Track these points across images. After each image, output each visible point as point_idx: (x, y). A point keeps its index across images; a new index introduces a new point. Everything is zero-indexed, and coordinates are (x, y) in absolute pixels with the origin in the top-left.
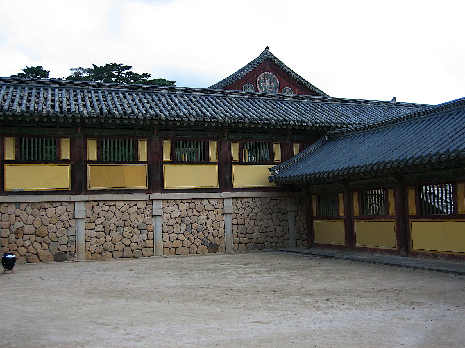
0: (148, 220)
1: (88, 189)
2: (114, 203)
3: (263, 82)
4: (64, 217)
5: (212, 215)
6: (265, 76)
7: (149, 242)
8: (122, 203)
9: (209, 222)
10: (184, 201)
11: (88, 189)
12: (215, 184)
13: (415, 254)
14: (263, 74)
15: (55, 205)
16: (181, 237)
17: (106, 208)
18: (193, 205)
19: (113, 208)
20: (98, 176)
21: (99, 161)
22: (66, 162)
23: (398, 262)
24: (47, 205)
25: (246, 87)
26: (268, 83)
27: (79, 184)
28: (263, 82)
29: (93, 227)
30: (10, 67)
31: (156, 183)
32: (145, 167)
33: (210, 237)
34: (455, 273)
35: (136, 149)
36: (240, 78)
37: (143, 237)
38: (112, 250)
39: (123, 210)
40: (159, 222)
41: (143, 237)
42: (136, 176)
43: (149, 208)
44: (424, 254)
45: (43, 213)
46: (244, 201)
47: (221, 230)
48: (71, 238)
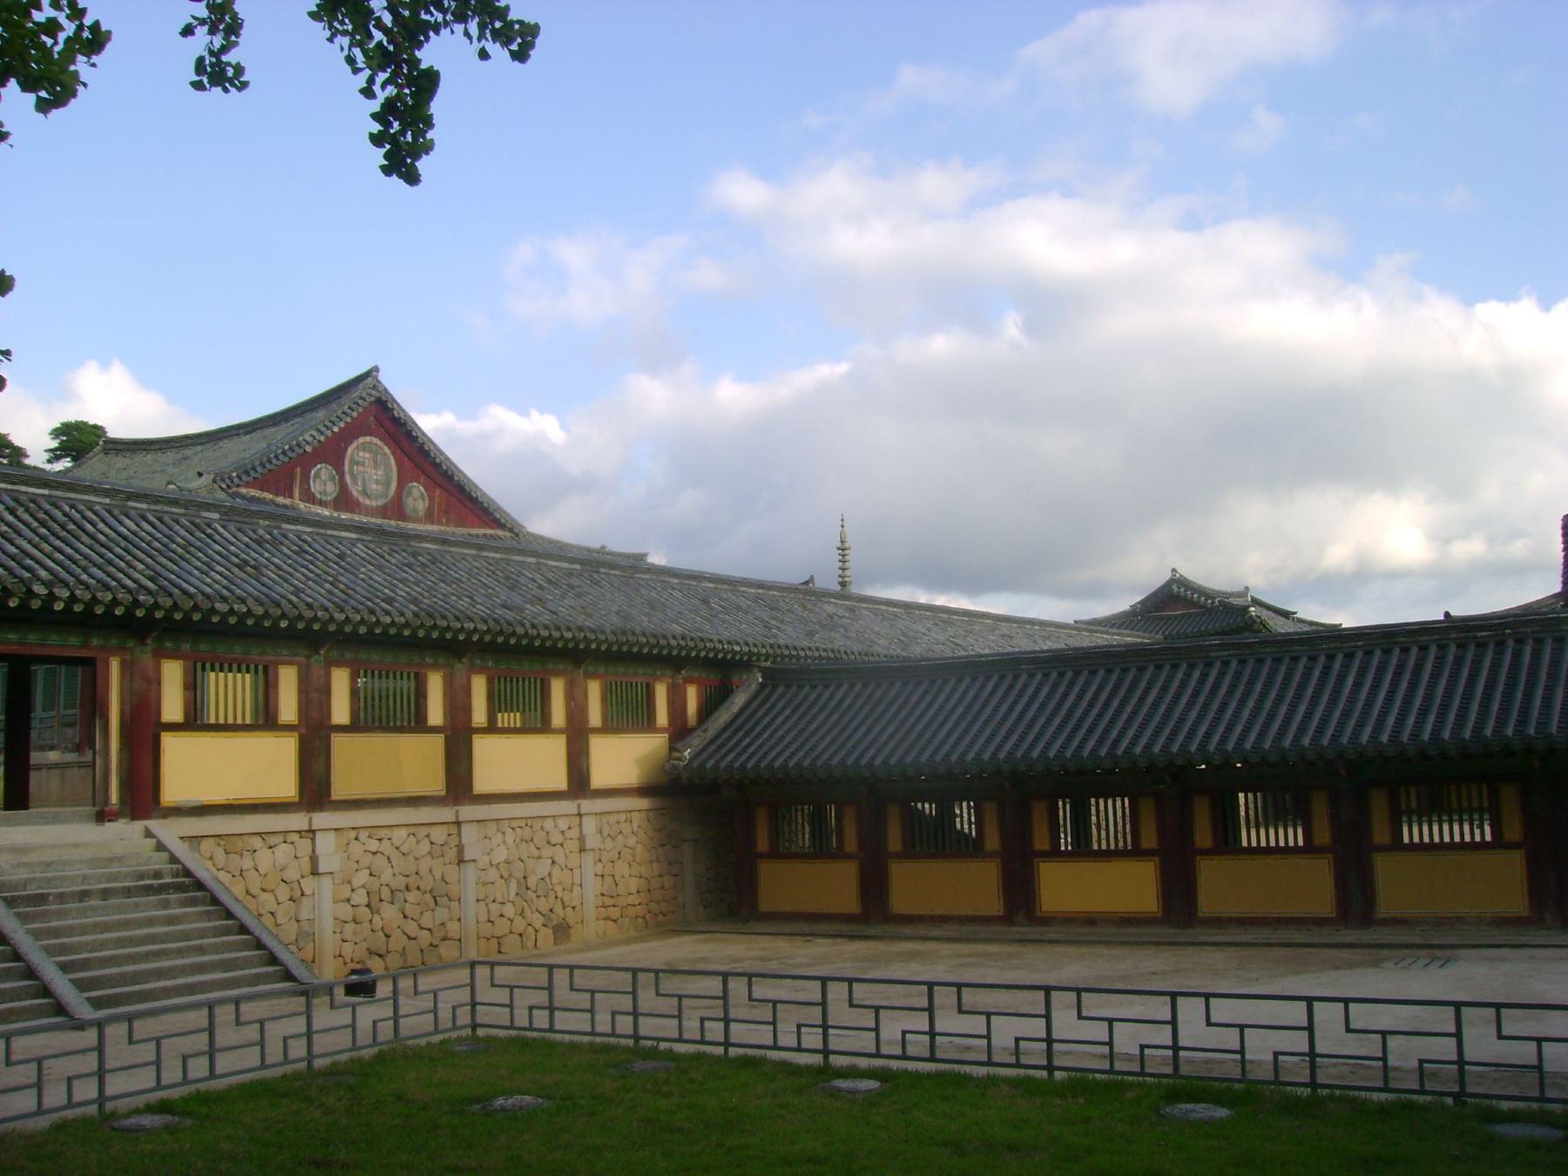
0: (452, 872)
1: (334, 797)
2: (388, 832)
3: (358, 463)
4: (292, 874)
5: (559, 854)
6: (364, 447)
7: (453, 928)
8: (404, 832)
9: (556, 872)
10: (514, 824)
11: (334, 797)
12: (561, 784)
13: (1047, 921)
14: (361, 440)
15: (272, 840)
16: (509, 910)
17: (373, 845)
18: (527, 833)
19: (386, 847)
20: (358, 761)
21: (354, 727)
22: (288, 728)
23: (1036, 936)
24: (257, 842)
25: (317, 475)
26: (371, 468)
27: (315, 789)
28: (358, 463)
29: (348, 894)
30: (3, 432)
31: (459, 784)
32: (439, 740)
33: (558, 908)
34: (1171, 944)
35: (421, 694)
36: (308, 449)
37: (442, 914)
38: (383, 952)
39: (405, 849)
40: (470, 872)
41: (442, 914)
42: (416, 760)
43: (454, 841)
44: (1068, 920)
45: (247, 863)
46: (613, 819)
47: (577, 889)
48: (306, 927)
